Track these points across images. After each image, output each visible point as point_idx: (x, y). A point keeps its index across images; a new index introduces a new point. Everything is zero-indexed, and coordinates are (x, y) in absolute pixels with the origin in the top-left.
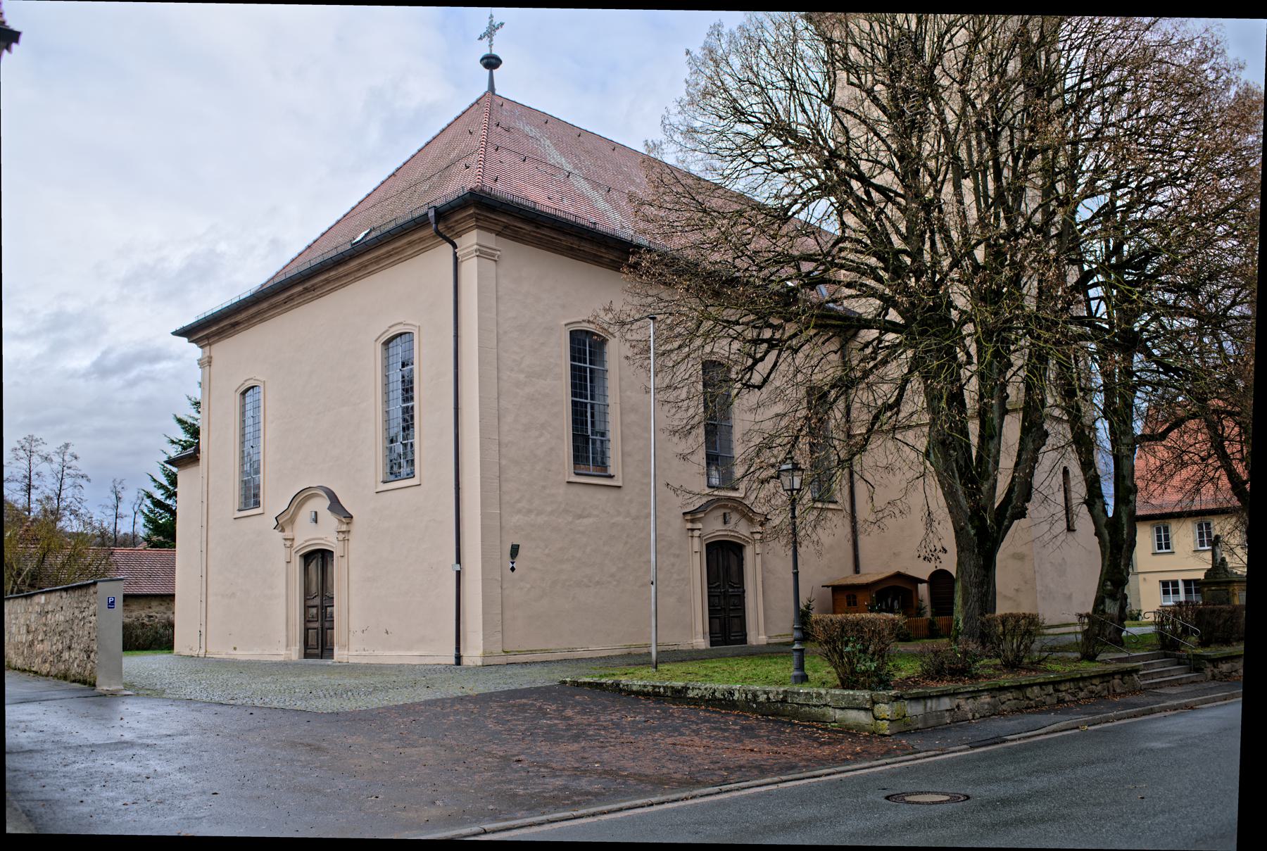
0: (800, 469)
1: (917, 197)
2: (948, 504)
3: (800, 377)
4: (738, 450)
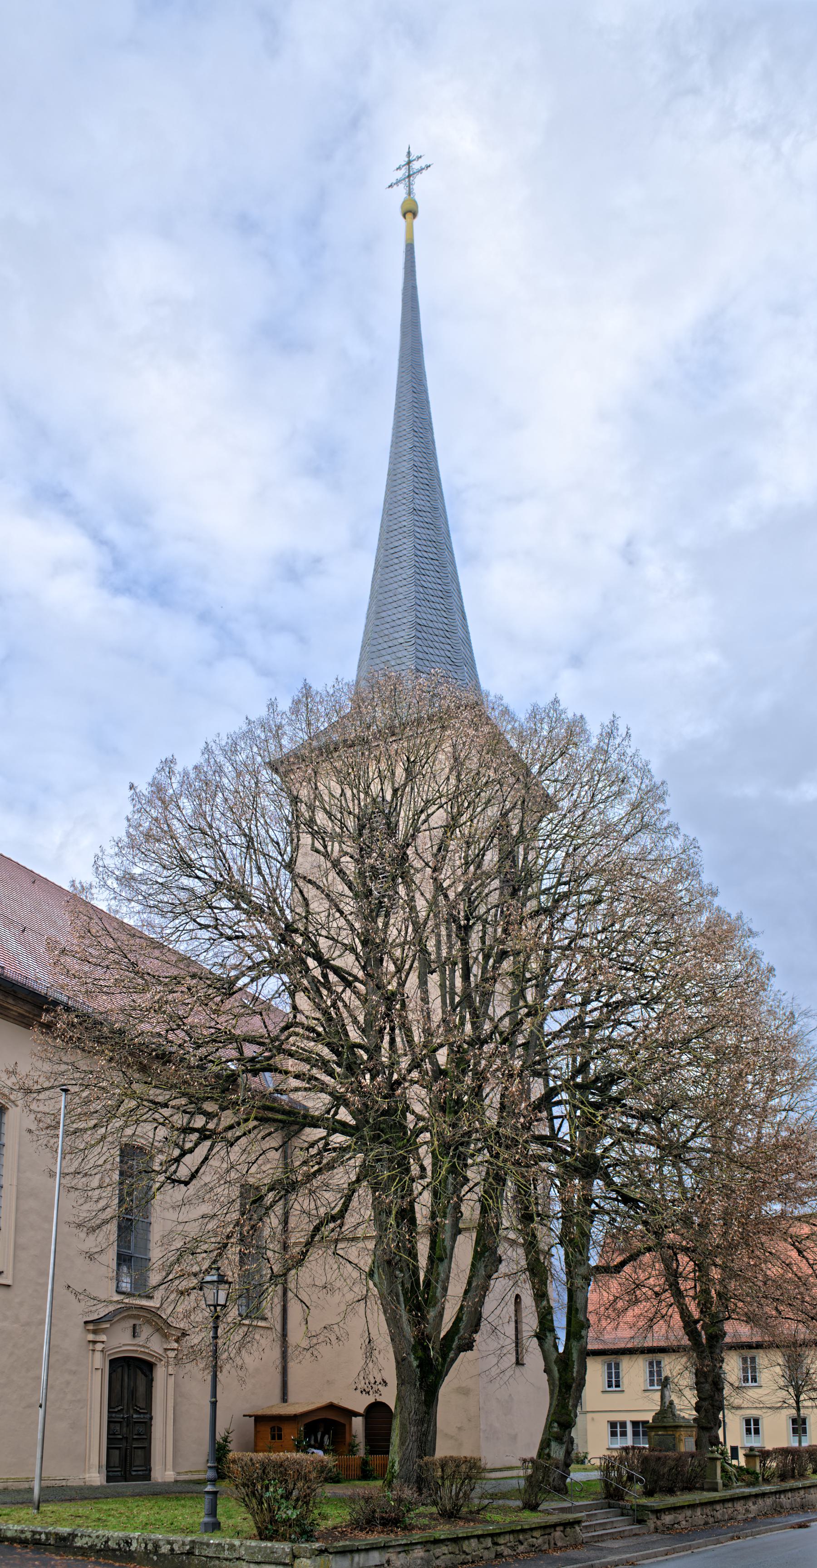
0: (227, 1282)
1: (379, 988)
2: (390, 1331)
3: (233, 1175)
4: (156, 1254)
